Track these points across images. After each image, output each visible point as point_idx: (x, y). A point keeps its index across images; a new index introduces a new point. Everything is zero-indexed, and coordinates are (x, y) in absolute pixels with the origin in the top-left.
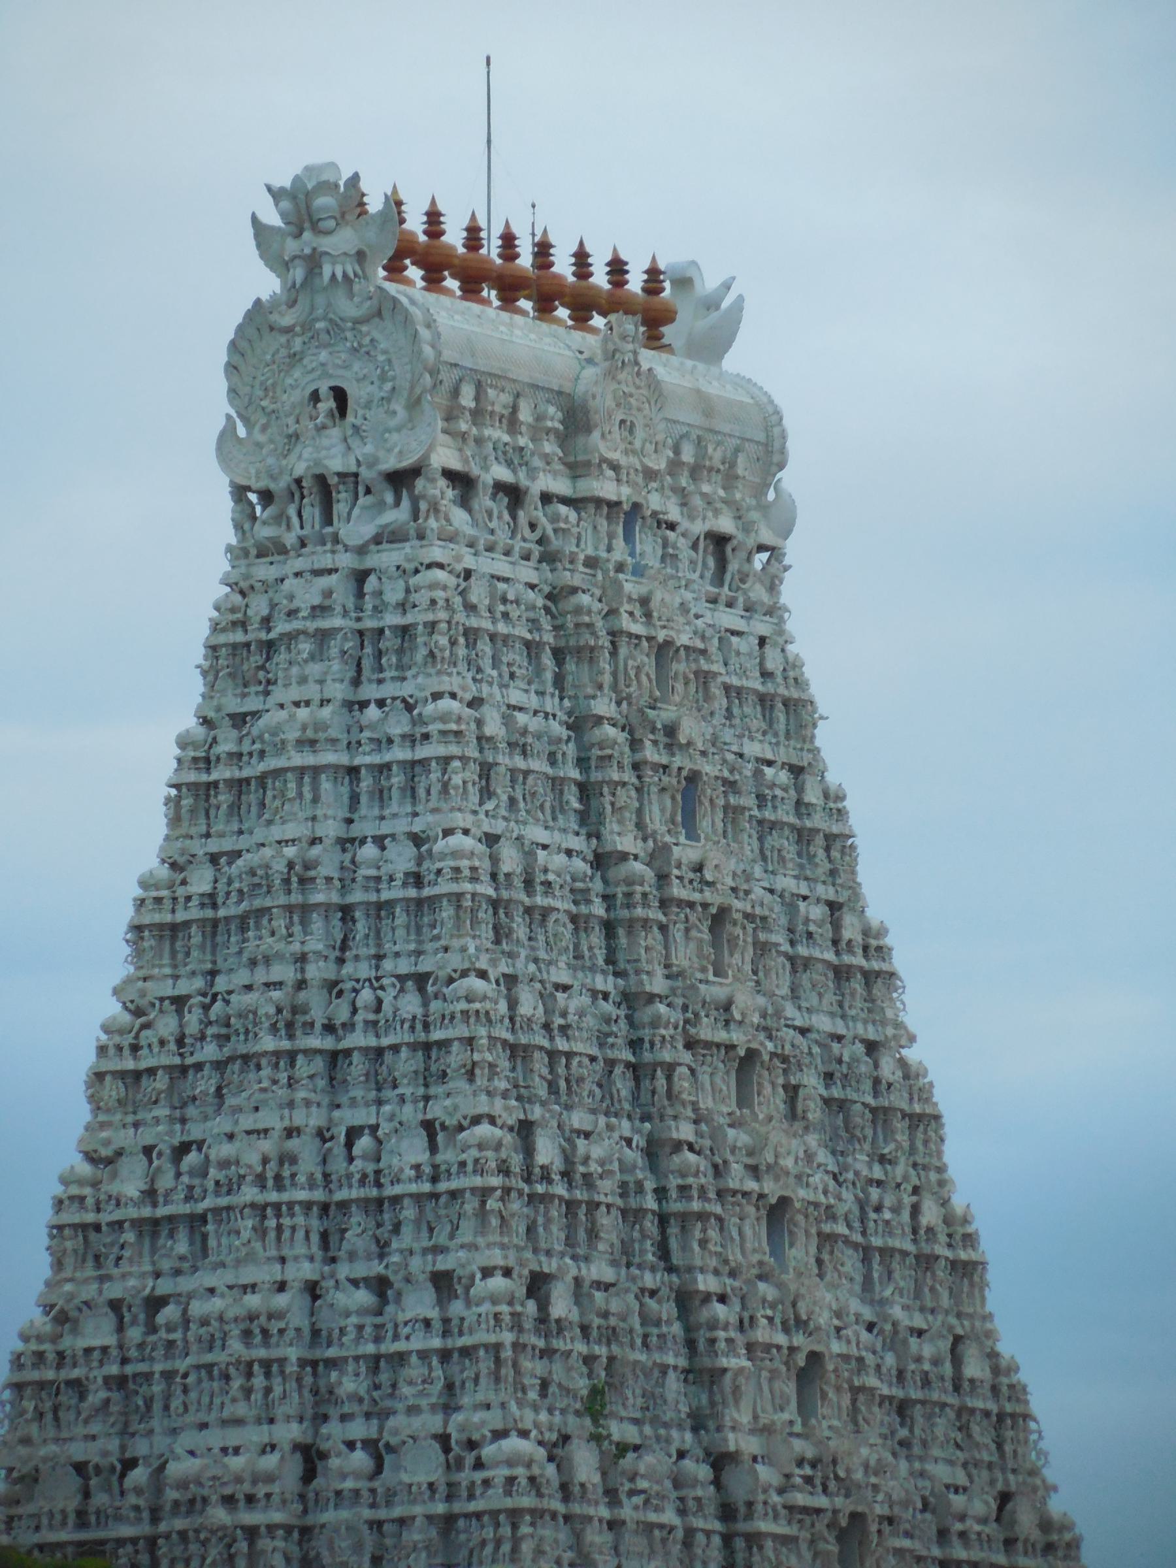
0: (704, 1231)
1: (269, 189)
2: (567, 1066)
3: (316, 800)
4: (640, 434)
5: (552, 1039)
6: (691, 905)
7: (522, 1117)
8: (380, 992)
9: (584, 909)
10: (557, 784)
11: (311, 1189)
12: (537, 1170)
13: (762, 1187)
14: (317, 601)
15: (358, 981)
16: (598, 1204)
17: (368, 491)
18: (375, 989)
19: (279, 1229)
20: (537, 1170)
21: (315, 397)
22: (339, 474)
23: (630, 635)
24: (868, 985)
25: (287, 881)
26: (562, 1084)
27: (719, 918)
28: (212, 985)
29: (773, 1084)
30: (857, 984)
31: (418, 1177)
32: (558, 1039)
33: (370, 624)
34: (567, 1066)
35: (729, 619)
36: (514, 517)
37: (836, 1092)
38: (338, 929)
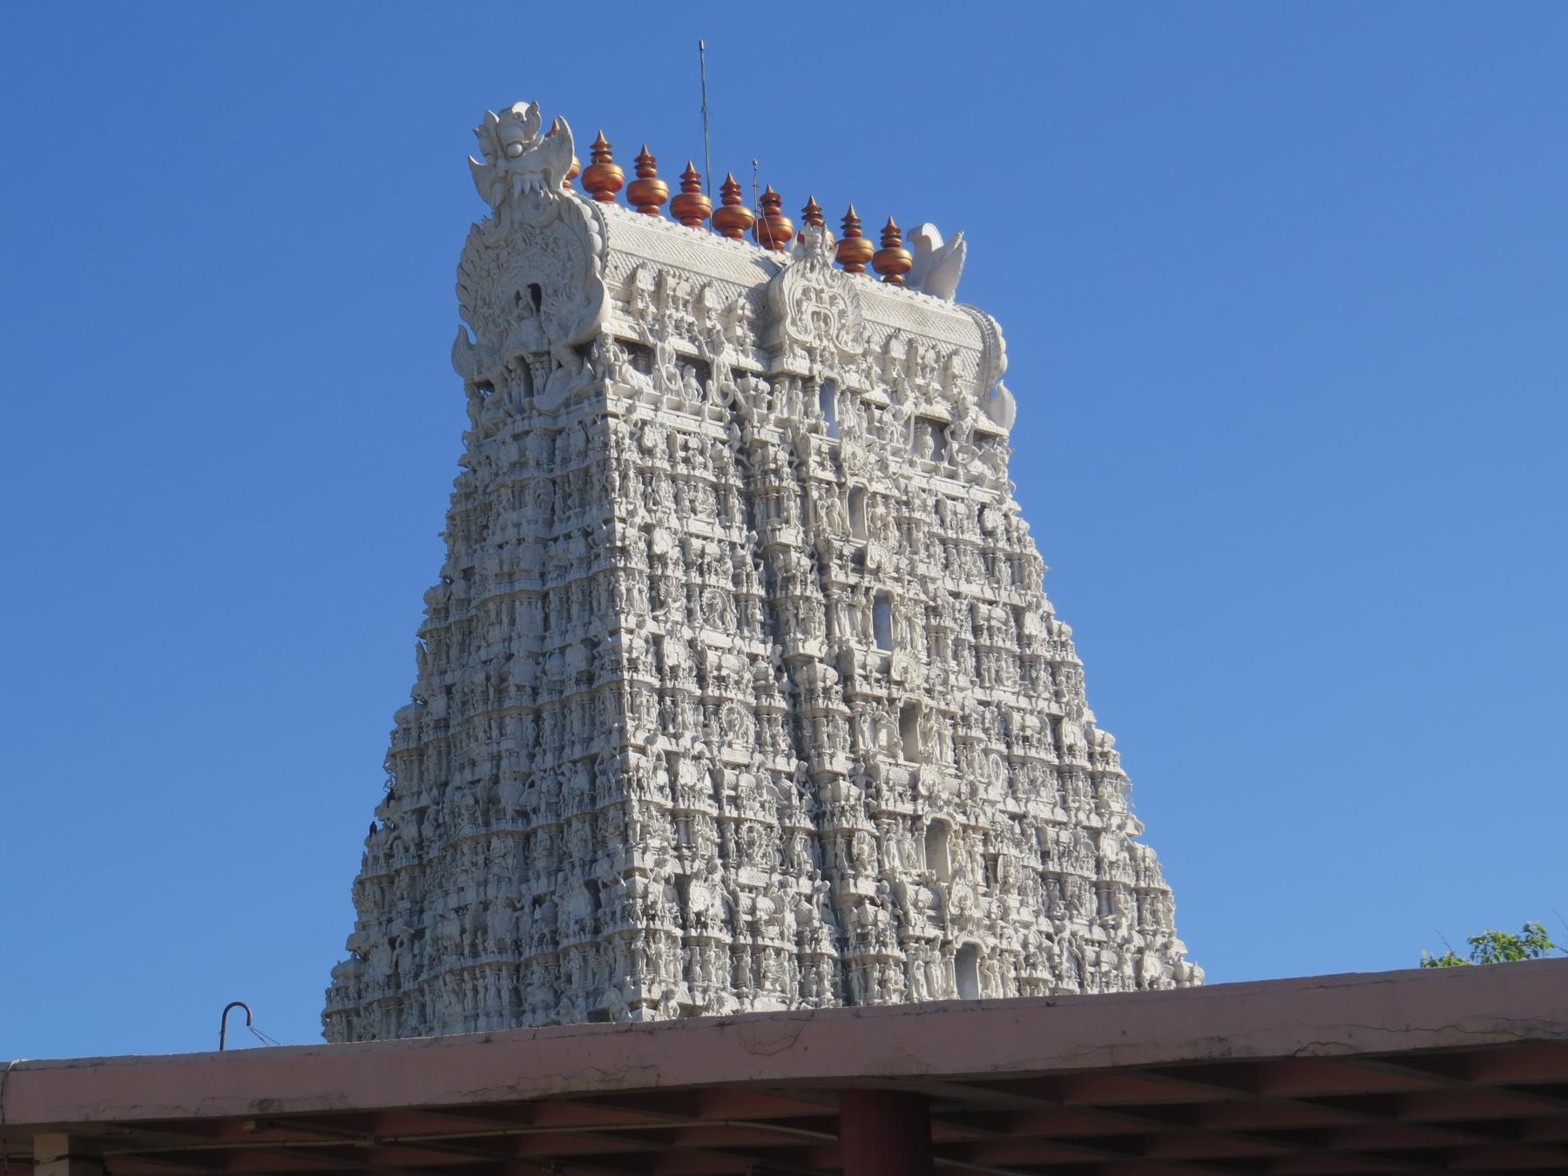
0: (883, 972)
2: (737, 832)
3: (513, 622)
4: (834, 326)
5: (721, 808)
6: (878, 700)
7: (680, 871)
9: (765, 702)
10: (740, 601)
11: (500, 953)
12: (692, 916)
13: (945, 935)
16: (765, 948)
17: (560, 366)
19: (475, 990)
20: (692, 916)
21: (518, 297)
22: (535, 354)
23: (820, 481)
24: (1095, 785)
26: (732, 846)
27: (909, 714)
29: (970, 854)
30: (1083, 785)
31: (583, 929)
32: (727, 808)
33: (558, 472)
34: (737, 832)
35: (943, 486)
36: (703, 385)
37: (1053, 866)
38: (530, 730)
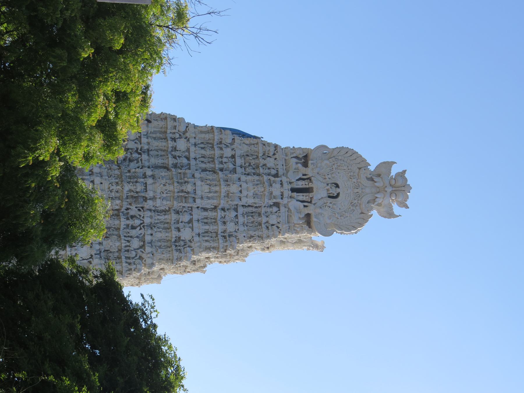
1: (404, 172)
8: (139, 228)
14: (274, 194)
15: (143, 217)
18: (140, 225)
25: (182, 191)
28: (144, 152)
